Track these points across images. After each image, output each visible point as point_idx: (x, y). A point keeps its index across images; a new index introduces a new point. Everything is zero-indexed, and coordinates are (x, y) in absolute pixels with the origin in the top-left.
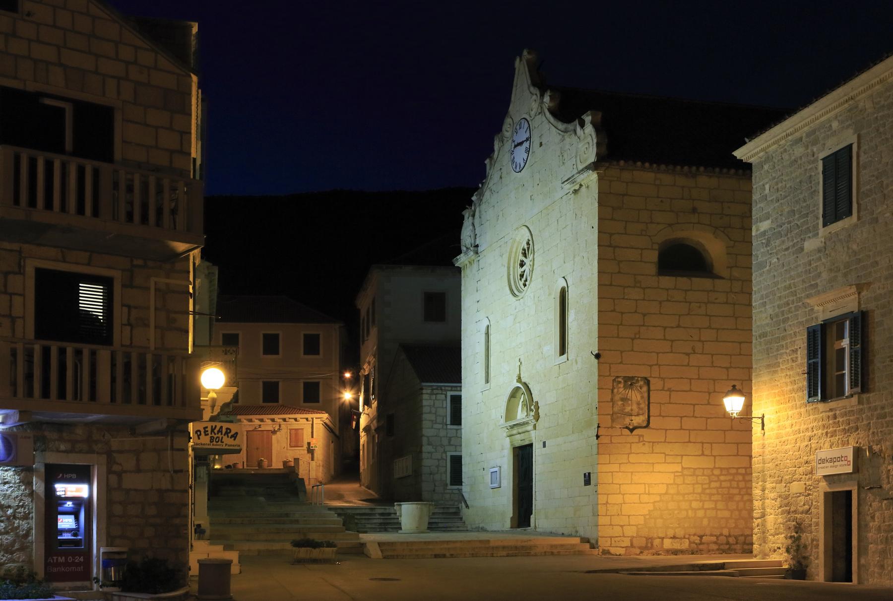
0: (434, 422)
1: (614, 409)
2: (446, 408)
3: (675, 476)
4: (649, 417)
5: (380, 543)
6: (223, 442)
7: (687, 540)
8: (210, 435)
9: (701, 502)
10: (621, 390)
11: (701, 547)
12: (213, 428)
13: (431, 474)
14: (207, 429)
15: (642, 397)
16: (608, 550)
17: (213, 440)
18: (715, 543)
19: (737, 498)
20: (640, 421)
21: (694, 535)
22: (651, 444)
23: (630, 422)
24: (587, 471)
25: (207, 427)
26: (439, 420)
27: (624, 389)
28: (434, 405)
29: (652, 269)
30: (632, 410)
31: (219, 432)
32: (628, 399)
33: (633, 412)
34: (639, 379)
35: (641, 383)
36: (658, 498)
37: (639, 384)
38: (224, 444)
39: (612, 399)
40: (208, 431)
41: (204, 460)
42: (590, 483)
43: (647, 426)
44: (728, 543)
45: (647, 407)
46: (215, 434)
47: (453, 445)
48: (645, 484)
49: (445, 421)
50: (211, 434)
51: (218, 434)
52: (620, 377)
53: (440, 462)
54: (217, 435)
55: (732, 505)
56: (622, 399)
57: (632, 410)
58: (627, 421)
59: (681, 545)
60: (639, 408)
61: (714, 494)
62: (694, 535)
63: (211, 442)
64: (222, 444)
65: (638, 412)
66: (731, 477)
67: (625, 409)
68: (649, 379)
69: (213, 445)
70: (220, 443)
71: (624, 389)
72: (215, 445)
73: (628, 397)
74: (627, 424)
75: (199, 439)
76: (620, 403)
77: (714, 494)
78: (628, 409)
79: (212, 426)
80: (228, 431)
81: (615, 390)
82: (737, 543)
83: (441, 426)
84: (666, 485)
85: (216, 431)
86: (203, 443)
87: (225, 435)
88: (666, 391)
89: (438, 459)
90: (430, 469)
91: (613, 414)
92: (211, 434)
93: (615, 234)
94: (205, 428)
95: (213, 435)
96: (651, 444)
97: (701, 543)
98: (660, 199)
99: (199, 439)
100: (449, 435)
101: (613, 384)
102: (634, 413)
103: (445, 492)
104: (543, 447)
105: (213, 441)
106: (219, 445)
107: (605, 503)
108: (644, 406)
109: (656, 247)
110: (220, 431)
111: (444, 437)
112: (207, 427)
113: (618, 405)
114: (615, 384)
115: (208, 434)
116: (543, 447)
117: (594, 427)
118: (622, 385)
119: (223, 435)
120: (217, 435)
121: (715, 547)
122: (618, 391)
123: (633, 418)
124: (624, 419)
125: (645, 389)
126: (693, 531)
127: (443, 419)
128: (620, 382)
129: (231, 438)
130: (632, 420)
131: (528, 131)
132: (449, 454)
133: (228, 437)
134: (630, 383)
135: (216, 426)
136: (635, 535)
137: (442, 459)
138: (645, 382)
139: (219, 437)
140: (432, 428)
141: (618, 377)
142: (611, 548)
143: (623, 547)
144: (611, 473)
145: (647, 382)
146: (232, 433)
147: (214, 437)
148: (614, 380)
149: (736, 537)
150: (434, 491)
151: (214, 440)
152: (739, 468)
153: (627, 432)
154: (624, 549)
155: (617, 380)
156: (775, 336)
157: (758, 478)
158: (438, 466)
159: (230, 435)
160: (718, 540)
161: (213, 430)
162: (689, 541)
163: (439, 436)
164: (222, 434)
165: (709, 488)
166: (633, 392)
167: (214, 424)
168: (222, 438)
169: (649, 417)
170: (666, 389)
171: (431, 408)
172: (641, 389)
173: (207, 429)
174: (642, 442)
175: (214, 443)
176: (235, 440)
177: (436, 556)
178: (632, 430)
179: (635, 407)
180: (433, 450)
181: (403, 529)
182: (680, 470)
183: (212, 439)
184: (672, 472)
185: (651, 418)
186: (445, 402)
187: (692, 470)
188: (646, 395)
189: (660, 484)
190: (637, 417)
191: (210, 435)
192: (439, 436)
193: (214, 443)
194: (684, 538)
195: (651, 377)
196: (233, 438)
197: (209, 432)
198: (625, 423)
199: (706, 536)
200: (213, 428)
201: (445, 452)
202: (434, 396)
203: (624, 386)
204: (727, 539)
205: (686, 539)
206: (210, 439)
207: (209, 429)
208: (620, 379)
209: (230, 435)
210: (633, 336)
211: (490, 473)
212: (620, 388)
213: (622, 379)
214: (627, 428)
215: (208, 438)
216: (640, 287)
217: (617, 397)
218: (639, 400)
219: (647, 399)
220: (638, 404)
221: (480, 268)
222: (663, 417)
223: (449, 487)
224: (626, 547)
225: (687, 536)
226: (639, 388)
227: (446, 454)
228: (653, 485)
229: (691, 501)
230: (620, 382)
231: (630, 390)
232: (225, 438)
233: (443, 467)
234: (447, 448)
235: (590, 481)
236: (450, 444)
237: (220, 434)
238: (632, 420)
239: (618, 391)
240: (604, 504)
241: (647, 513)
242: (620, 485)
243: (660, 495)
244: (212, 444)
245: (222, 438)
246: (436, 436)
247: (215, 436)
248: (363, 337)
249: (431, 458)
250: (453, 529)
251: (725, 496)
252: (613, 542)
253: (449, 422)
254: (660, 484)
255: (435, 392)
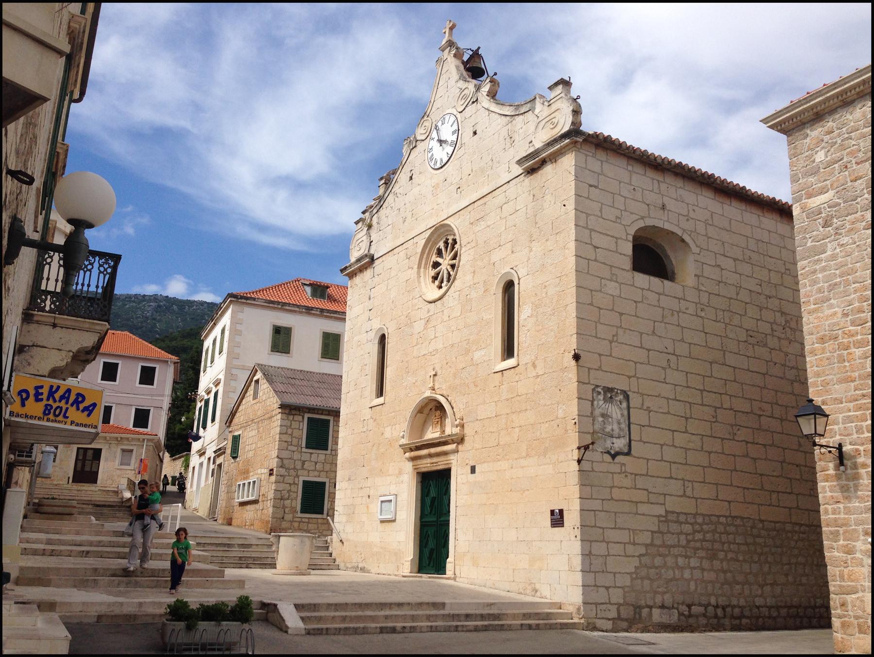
0: (290, 443)
1: (595, 427)
2: (302, 429)
3: (659, 521)
4: (630, 440)
5: (298, 605)
6: (68, 417)
7: (676, 611)
8: (45, 402)
9: (686, 558)
10: (601, 402)
11: (691, 621)
12: (54, 390)
13: (281, 499)
14: (40, 391)
15: (622, 415)
16: (594, 623)
17: (49, 411)
18: (704, 615)
19: (721, 555)
20: (622, 446)
21: (683, 603)
22: (633, 476)
23: (612, 445)
24: (556, 508)
25: (42, 387)
26: (295, 441)
27: (604, 402)
28: (291, 425)
29: (627, 263)
30: (613, 430)
31: (62, 398)
32: (609, 416)
33: (614, 432)
34: (619, 392)
35: (621, 397)
36: (643, 551)
37: (618, 398)
38: (69, 420)
39: (592, 413)
40: (42, 394)
41: (27, 456)
42: (563, 524)
43: (628, 453)
44: (716, 616)
45: (627, 429)
46: (55, 401)
47: (306, 470)
48: (629, 529)
49: (300, 443)
50: (48, 400)
51: (60, 401)
52: (600, 386)
53: (292, 486)
54: (57, 404)
55: (717, 564)
56: (603, 415)
57: (613, 430)
58: (608, 444)
59: (670, 618)
60: (620, 429)
61: (698, 549)
62: (683, 603)
63: (44, 414)
64: (65, 420)
65: (619, 434)
66: (713, 527)
67: (605, 428)
68: (629, 393)
69: (48, 420)
70: (60, 418)
71: (604, 402)
72: (52, 421)
73: (609, 414)
74: (608, 448)
75: (23, 405)
76: (601, 419)
77: (698, 549)
78: (608, 429)
79: (52, 387)
80: (80, 399)
81: (595, 403)
82: (725, 617)
83: (295, 449)
84: (650, 533)
85: (57, 396)
86: (29, 414)
87: (72, 405)
88: (645, 410)
89: (290, 484)
90: (281, 493)
91: (593, 433)
92: (48, 400)
93: (591, 215)
94: (37, 388)
95: (51, 402)
96: (633, 476)
97: (690, 616)
98: (633, 187)
99: (23, 405)
100: (302, 459)
101: (593, 394)
102: (616, 433)
103: (294, 520)
104: (472, 473)
105: (49, 414)
106: (59, 422)
107: (588, 553)
108: (624, 426)
109: (631, 238)
110: (65, 397)
111: (298, 460)
112: (42, 387)
113: (598, 422)
114: (595, 395)
115: (42, 400)
116: (472, 473)
117: (569, 449)
118: (601, 397)
119: (68, 406)
120: (57, 404)
121: (703, 621)
122: (598, 404)
123: (615, 440)
124: (605, 441)
125: (624, 405)
126: (680, 598)
127: (298, 442)
128: (599, 393)
129: (83, 411)
130: (613, 443)
131: (456, 124)
132: (302, 479)
133: (78, 409)
134: (609, 396)
135: (58, 387)
136: (622, 601)
137: (294, 483)
138: (624, 397)
139: (61, 408)
140: (287, 449)
141: (597, 386)
142: (597, 621)
143: (609, 619)
144: (593, 512)
145: (627, 397)
146: (86, 403)
147: (52, 407)
148: (593, 390)
149: (724, 608)
150: (283, 518)
151: (52, 411)
152: (720, 516)
153: (608, 458)
154: (611, 622)
155: (596, 390)
156: (855, 338)
157: (836, 534)
158: (289, 491)
159: (82, 406)
160: (706, 612)
161: (51, 393)
162: (678, 612)
163: (293, 459)
164: (67, 403)
165: (694, 540)
166: (613, 407)
167: (56, 382)
168: (67, 409)
169: (630, 440)
170: (645, 408)
171: (287, 429)
172: (621, 404)
173: (40, 391)
174: (624, 473)
175: (51, 416)
176: (89, 415)
177: (382, 630)
178: (613, 457)
179: (615, 427)
180: (286, 474)
181: (278, 566)
182: (663, 513)
183: (47, 410)
184: (656, 516)
185: (633, 443)
186: (301, 424)
187: (676, 515)
188: (626, 413)
189: (645, 530)
190: (618, 440)
191: (45, 402)
192: (293, 459)
193: (51, 416)
194: (673, 607)
195: (630, 391)
196: (86, 413)
197: (45, 396)
198: (606, 446)
199: (695, 605)
200: (54, 390)
201: (298, 476)
202: (292, 416)
203: (604, 399)
204: (715, 610)
205: (675, 608)
206: (43, 408)
207: (45, 391)
208: (599, 390)
209: (82, 406)
210: (611, 338)
211: (380, 502)
212: (600, 400)
213: (602, 389)
214: (608, 453)
215: (41, 406)
216: (617, 282)
217: (597, 412)
218: (619, 418)
219: (627, 418)
220: (619, 423)
221: (375, 274)
222: (645, 442)
223: (300, 515)
224: (613, 619)
225: (675, 606)
226: (619, 403)
227: (298, 478)
228: (638, 531)
229: (676, 556)
230: (599, 393)
231: (610, 404)
232: (72, 411)
233: (294, 492)
234: (300, 472)
235: (563, 521)
236: (303, 468)
237: (63, 401)
238: (613, 443)
239: (598, 404)
240: (587, 555)
241: (633, 570)
242: (603, 529)
243: (647, 545)
244: (45, 418)
245: (67, 409)
246: (290, 458)
247: (55, 405)
248: (205, 366)
249: (283, 482)
250: (323, 567)
251: (709, 552)
252: (599, 612)
253: (304, 445)
254: (645, 530)
255: (293, 412)
